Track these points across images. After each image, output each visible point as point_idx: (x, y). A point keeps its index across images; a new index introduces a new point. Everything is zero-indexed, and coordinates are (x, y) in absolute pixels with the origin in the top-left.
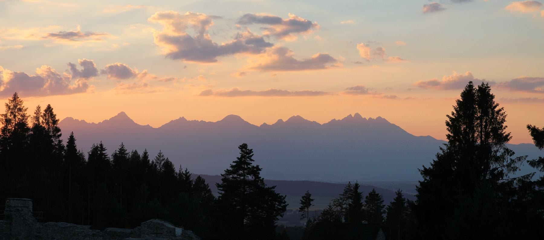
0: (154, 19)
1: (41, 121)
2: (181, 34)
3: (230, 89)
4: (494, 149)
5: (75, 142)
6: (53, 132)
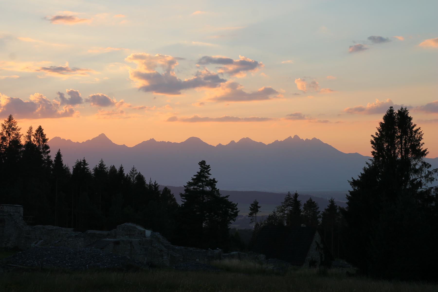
0: (130, 59)
1: (32, 140)
2: (152, 72)
3: (191, 116)
5: (62, 157)
6: (43, 149)
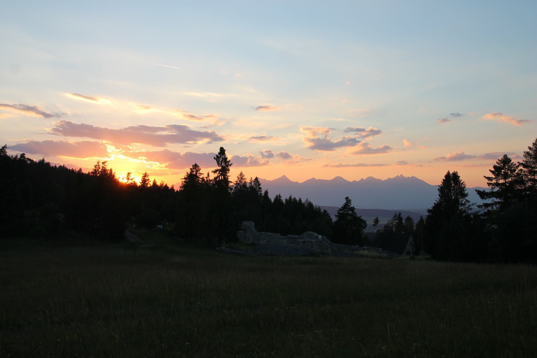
3: (337, 164)
4: (461, 200)
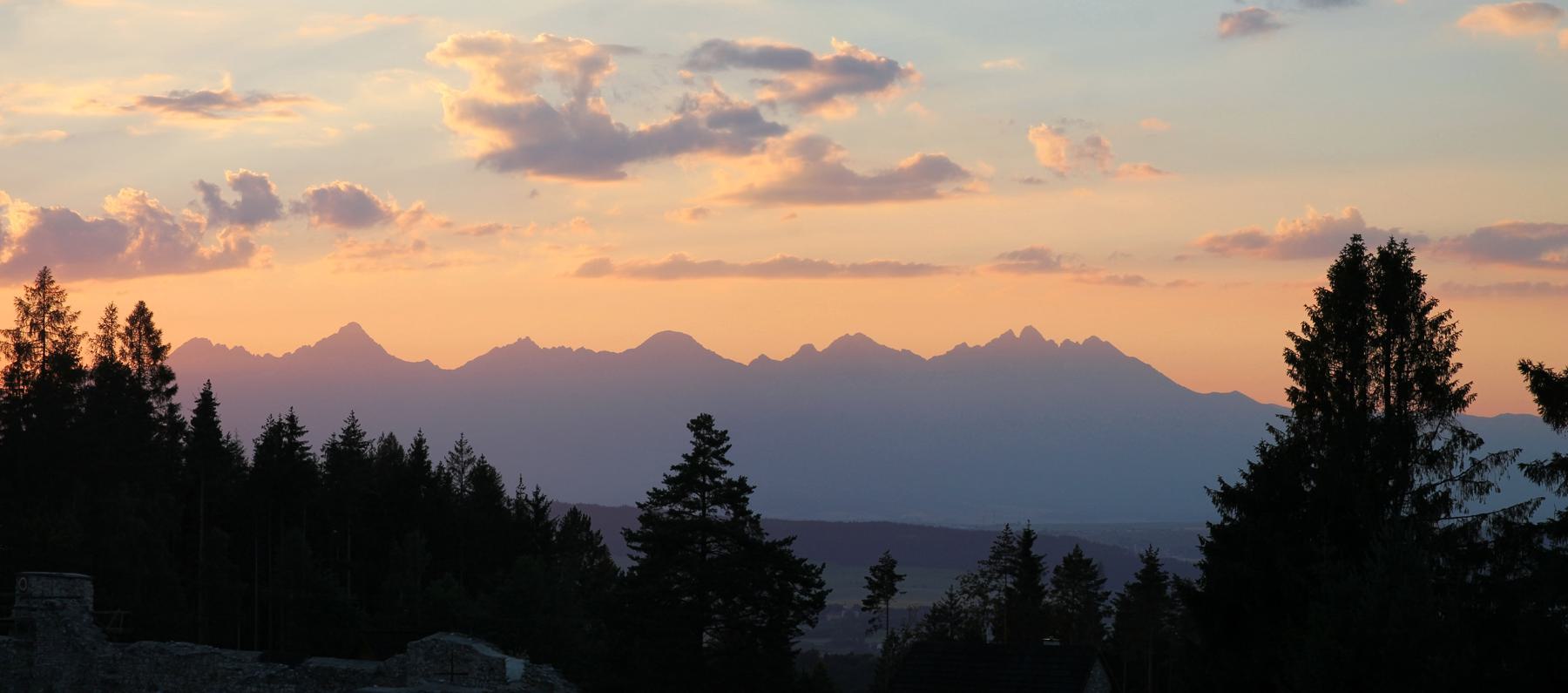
0: (445, 53)
1: (117, 350)
2: (522, 99)
3: (662, 257)
4: (1425, 429)
5: (217, 409)
6: (153, 381)
